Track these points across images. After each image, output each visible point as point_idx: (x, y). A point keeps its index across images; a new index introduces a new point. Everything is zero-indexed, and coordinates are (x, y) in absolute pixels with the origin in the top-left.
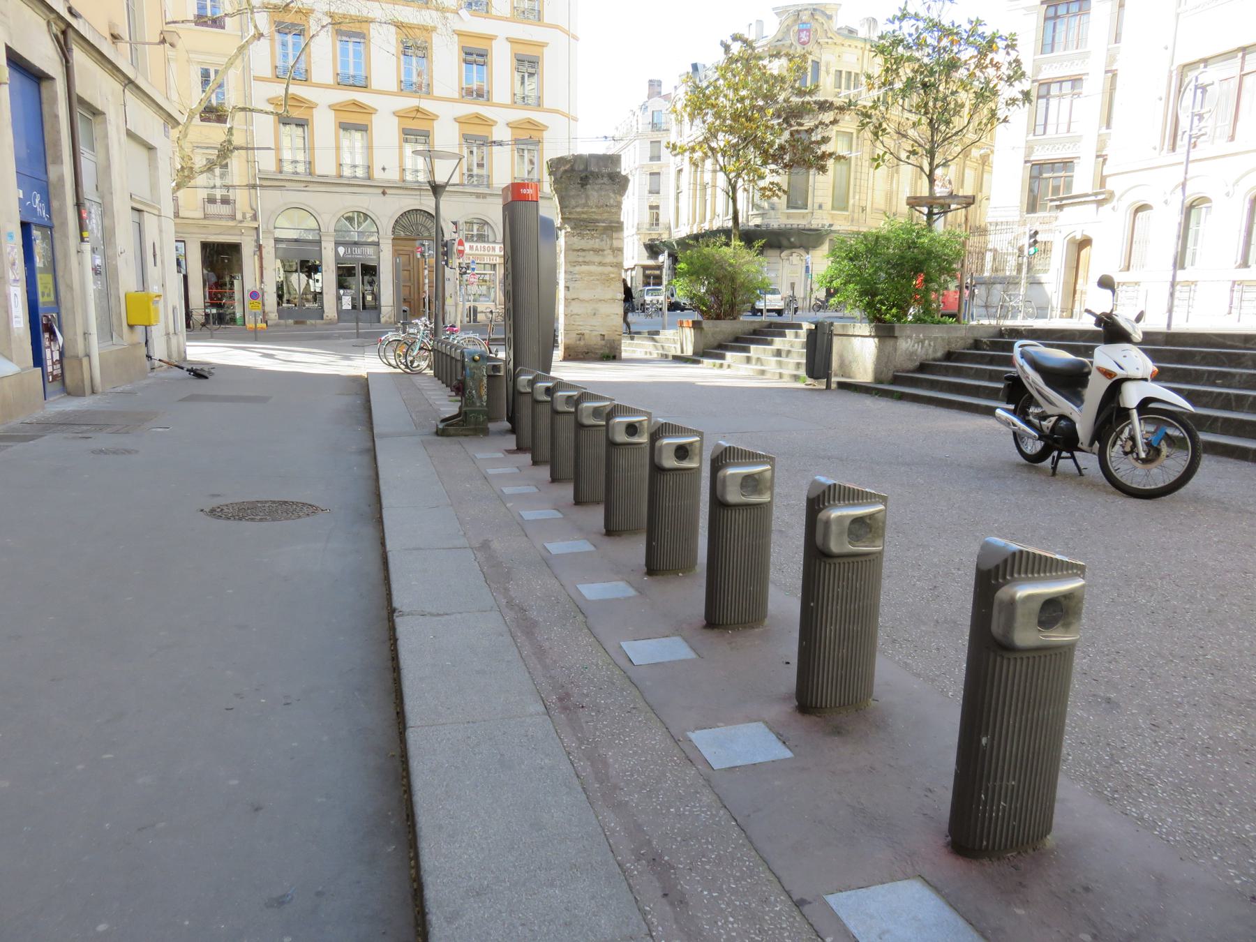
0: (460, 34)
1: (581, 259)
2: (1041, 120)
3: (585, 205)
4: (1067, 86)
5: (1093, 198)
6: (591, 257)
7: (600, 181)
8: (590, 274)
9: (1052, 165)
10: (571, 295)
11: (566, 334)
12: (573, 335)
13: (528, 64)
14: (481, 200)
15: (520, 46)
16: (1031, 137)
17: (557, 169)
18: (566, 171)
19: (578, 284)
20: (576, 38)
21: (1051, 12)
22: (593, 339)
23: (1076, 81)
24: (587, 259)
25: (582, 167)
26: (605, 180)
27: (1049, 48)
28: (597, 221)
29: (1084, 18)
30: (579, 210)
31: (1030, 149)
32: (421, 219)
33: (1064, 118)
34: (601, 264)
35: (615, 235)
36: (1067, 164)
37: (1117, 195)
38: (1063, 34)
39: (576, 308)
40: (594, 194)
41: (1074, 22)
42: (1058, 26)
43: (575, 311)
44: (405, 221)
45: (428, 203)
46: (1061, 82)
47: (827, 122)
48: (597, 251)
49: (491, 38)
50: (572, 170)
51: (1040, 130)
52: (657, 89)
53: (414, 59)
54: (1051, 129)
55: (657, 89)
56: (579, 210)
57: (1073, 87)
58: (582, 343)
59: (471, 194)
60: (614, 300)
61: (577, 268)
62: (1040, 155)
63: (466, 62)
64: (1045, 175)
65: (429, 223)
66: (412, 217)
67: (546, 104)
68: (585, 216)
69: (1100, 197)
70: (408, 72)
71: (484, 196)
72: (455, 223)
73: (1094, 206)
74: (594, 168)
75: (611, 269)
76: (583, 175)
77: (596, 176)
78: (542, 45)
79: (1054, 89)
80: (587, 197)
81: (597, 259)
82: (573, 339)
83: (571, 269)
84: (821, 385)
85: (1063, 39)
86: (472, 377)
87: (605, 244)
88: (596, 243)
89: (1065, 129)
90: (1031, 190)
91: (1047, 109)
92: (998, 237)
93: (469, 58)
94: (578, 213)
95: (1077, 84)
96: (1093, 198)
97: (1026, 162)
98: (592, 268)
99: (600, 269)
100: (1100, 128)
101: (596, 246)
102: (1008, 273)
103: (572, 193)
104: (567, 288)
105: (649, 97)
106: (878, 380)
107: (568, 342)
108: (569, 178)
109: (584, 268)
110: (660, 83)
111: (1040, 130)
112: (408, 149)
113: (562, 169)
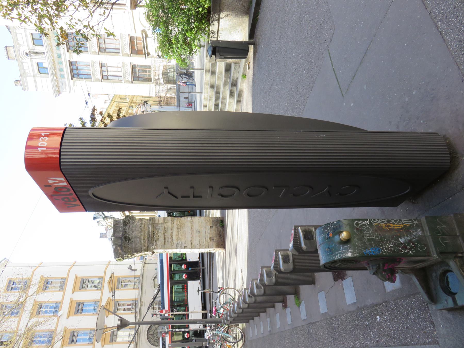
0: (69, 315)
1: (170, 240)
2: (117, 78)
3: (140, 238)
4: (104, 69)
5: (144, 39)
6: (168, 235)
7: (127, 230)
8: (177, 235)
9: (134, 73)
10: (189, 246)
11: (211, 247)
12: (211, 243)
13: (83, 284)
14: (143, 304)
15: (76, 289)
16: (123, 81)
17: (120, 254)
18: (122, 250)
19: (183, 241)
20: (75, 262)
21: (76, 76)
22: (213, 232)
23: (102, 65)
24: (170, 237)
25: (120, 241)
26: (127, 227)
27: (89, 76)
28: (149, 233)
29: (78, 63)
30: (143, 242)
31: (128, 81)
32: (151, 332)
33: (115, 69)
34: (172, 229)
35: (157, 222)
36: (133, 67)
37: (143, 28)
38: (85, 71)
39: (196, 242)
40: (134, 233)
41: (79, 67)
42: (81, 73)
43: (198, 243)
44: (152, 340)
45: (144, 328)
46: (102, 71)
47: (101, 117)
48: (165, 231)
49: (72, 301)
50: (121, 246)
51: (120, 78)
52: (104, 234)
53: (78, 337)
54: (120, 74)
55: (104, 234)
56: (143, 242)
57: (104, 67)
58: (215, 238)
59: (140, 308)
60: (191, 222)
61: (175, 242)
62: (130, 77)
63: (82, 311)
64: (137, 76)
65: (154, 328)
66: (150, 336)
67: (102, 275)
68: (146, 238)
69: (144, 36)
70: (84, 340)
71: (141, 302)
72: (153, 315)
73: (148, 38)
74: (121, 234)
75: (175, 224)
76: (124, 239)
77: (125, 232)
78: (76, 277)
79: (105, 73)
80: (136, 237)
81: (169, 231)
82: (213, 243)
83: (175, 245)
84: (251, 48)
85: (86, 71)
86: (379, 243)
87: (161, 227)
88: (161, 232)
89: (120, 69)
90: (142, 81)
91: (112, 76)
92: (161, 91)
93: (80, 311)
94: (144, 242)
95: (103, 65)
96: (144, 39)
97: (132, 83)
98: (174, 233)
99: (175, 229)
100: (119, 55)
101: (163, 232)
102: (175, 88)
103: (134, 246)
104: (185, 247)
105: (106, 237)
106: (247, 12)
107: (214, 246)
108: (125, 247)
109: (174, 238)
110: (101, 234)
111: (120, 78)
112: (119, 339)
113: (120, 251)
